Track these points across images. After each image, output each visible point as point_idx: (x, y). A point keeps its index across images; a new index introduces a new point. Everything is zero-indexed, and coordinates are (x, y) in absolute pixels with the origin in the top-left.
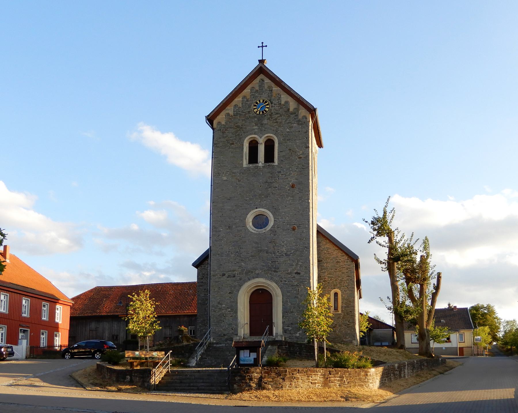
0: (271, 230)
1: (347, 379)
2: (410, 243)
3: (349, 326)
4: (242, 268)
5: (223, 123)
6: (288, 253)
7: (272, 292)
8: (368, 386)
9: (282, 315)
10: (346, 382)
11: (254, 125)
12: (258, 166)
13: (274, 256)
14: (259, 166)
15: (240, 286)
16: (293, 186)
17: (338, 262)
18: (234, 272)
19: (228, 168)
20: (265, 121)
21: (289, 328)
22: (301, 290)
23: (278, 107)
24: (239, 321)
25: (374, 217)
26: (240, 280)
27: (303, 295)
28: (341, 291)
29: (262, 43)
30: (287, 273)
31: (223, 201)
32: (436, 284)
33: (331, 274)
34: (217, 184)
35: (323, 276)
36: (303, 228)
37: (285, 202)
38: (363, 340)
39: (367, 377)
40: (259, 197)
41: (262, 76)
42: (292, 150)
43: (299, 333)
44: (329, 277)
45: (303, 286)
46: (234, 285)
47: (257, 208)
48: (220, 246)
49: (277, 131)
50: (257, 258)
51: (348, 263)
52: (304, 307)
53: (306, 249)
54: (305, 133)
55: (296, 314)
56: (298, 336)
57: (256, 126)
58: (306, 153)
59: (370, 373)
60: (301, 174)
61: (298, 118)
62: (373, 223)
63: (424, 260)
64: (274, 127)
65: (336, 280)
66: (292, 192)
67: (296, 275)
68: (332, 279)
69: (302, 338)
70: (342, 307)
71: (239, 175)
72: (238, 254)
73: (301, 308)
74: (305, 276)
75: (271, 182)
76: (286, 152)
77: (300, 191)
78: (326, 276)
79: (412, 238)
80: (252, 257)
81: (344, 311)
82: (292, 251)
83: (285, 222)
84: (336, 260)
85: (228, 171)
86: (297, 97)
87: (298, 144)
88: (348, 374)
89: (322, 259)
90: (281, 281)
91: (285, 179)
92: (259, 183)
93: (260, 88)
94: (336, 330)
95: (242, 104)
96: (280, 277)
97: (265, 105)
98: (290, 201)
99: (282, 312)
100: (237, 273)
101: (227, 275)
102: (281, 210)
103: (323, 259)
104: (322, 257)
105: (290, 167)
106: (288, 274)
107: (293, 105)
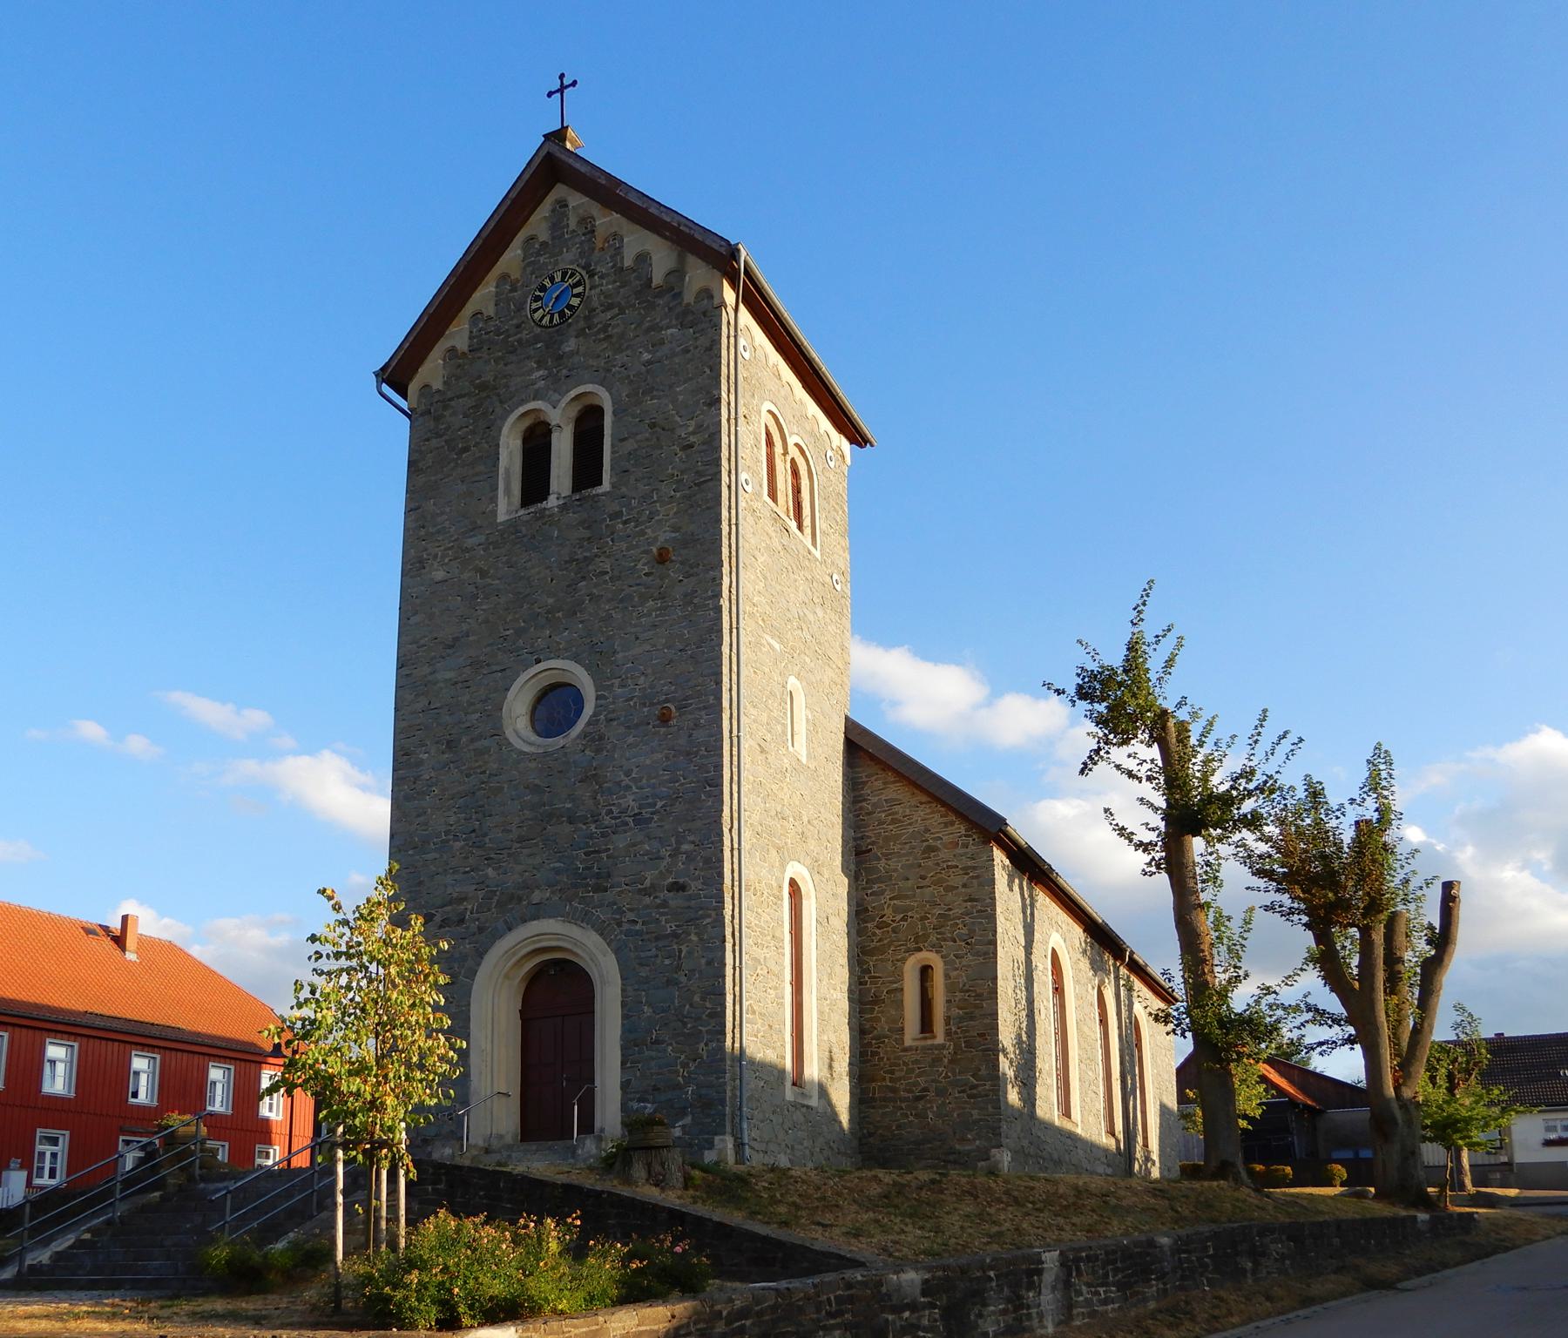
3: (975, 1091)
4: (488, 886)
5: (437, 385)
6: (643, 811)
9: (622, 1055)
12: (545, 509)
15: (480, 954)
16: (660, 555)
20: (571, 345)
21: (646, 1108)
23: (615, 282)
24: (472, 1089)
27: (694, 970)
29: (562, 76)
32: (1437, 924)
33: (907, 897)
35: (874, 908)
36: (699, 709)
41: (560, 191)
43: (680, 1123)
44: (896, 910)
45: (696, 934)
47: (540, 662)
48: (418, 816)
49: (609, 371)
50: (536, 845)
53: (708, 788)
56: (679, 1138)
57: (538, 369)
58: (708, 427)
60: (692, 506)
62: (1083, 693)
63: (1371, 834)
65: (923, 919)
66: (658, 581)
67: (672, 894)
68: (910, 914)
69: (691, 1145)
70: (948, 1020)
71: (482, 552)
74: (705, 897)
75: (586, 558)
77: (687, 569)
81: (956, 1033)
82: (659, 804)
83: (631, 699)
85: (450, 549)
87: (681, 398)
89: (869, 844)
90: (619, 924)
91: (634, 538)
92: (547, 568)
93: (556, 234)
99: (622, 1046)
100: (470, 907)
102: (620, 656)
106: (646, 892)
107: (662, 258)
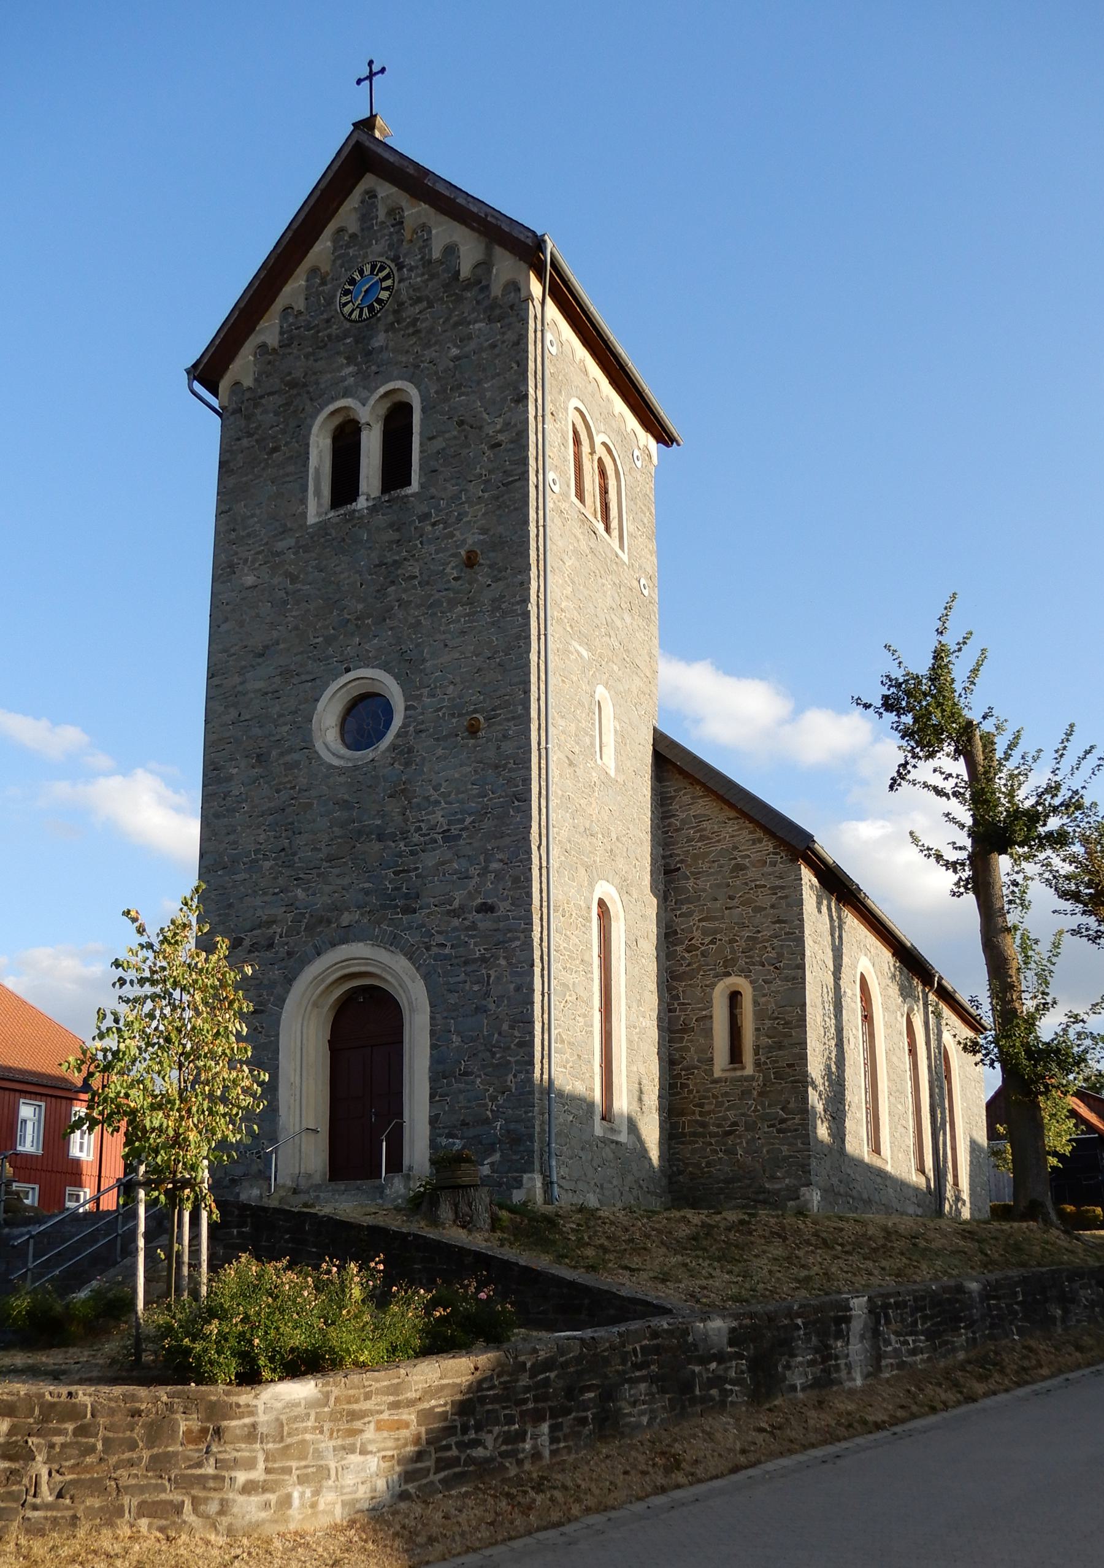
0: (393, 747)
1: (56, 1466)
2: (1058, 766)
3: (784, 1126)
5: (248, 382)
7: (406, 991)
8: (222, 1512)
10: (44, 1488)
11: (342, 365)
12: (354, 510)
13: (403, 848)
14: (358, 511)
15: (289, 980)
16: (469, 558)
17: (739, 868)
18: (268, 928)
19: (262, 540)
20: (380, 340)
22: (498, 978)
23: (423, 274)
25: (887, 676)
26: (289, 959)
28: (751, 982)
30: (449, 912)
31: (243, 663)
33: (714, 919)
34: (227, 604)
35: (683, 930)
36: (508, 720)
37: (442, 629)
38: (1092, 1182)
39: (214, 1449)
40: (356, 625)
41: (369, 181)
42: (467, 424)
44: (705, 932)
45: (505, 957)
46: (269, 979)
51: (776, 869)
52: (509, 1048)
53: (516, 803)
54: (515, 347)
55: (479, 1080)
56: (488, 1176)
57: (348, 364)
59: (247, 1420)
60: (499, 507)
61: (488, 297)
62: (889, 704)
64: (407, 352)
65: (732, 941)
68: (718, 936)
70: (757, 1050)
72: (286, 856)
73: (498, 1056)
75: (395, 561)
76: (447, 435)
77: (496, 573)
78: (695, 928)
79: (1065, 748)
80: (330, 861)
81: (765, 1063)
82: (468, 820)
83: (442, 708)
84: (732, 859)
86: (477, 215)
88: (70, 1427)
89: (678, 862)
90: (428, 949)
91: (443, 540)
94: (734, 1145)
95: (306, 299)
96: (424, 930)
97: (377, 282)
98: (460, 621)
99: (430, 1078)
100: (279, 930)
101: (247, 943)
103: (682, 862)
104: (679, 855)
105: (461, 491)
106: (454, 914)
